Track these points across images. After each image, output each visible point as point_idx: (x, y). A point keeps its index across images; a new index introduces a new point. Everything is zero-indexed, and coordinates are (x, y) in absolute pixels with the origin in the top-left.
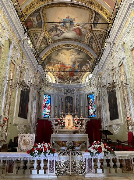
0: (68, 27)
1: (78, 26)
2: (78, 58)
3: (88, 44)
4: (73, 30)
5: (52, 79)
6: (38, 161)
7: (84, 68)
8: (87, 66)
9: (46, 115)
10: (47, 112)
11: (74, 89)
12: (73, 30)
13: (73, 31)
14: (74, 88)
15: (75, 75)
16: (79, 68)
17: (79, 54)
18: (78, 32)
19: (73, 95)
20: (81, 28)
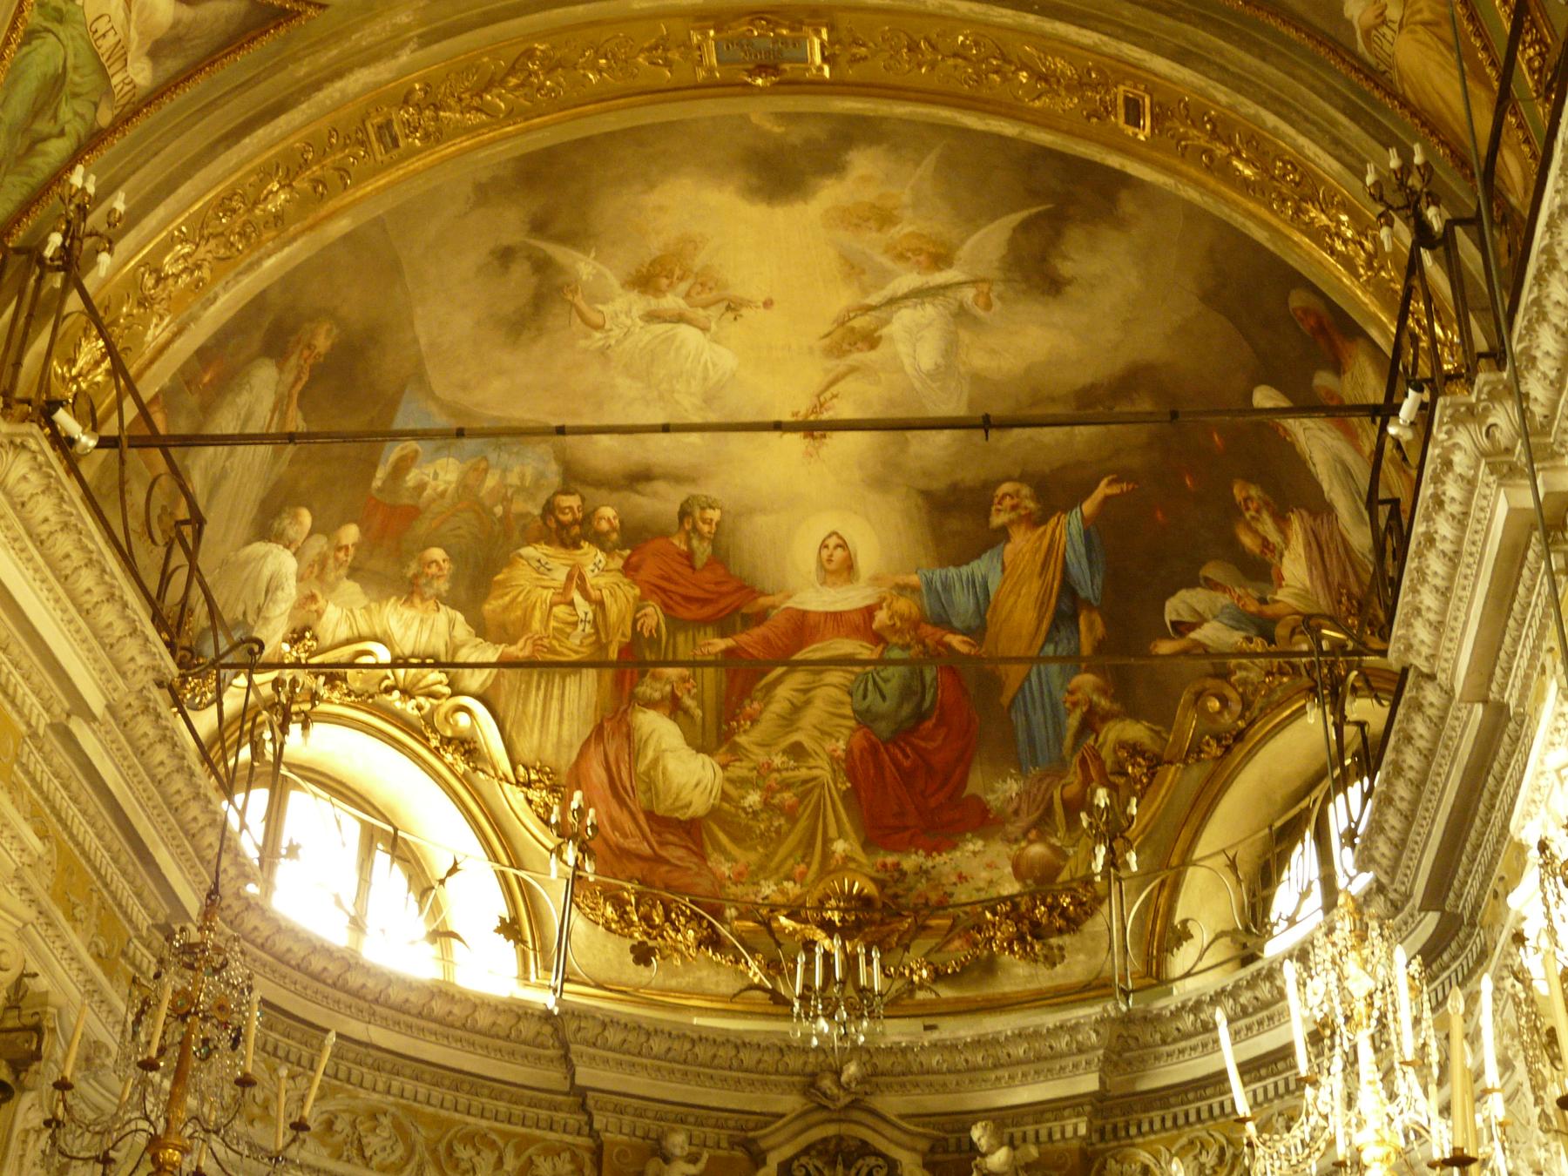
5: (131, 883)
6: (1127, 99)
7: (1211, 633)
8: (1260, 570)
11: (979, 1134)
14: (964, 1120)
15: (983, 821)
16: (1090, 629)
17: (1052, 286)
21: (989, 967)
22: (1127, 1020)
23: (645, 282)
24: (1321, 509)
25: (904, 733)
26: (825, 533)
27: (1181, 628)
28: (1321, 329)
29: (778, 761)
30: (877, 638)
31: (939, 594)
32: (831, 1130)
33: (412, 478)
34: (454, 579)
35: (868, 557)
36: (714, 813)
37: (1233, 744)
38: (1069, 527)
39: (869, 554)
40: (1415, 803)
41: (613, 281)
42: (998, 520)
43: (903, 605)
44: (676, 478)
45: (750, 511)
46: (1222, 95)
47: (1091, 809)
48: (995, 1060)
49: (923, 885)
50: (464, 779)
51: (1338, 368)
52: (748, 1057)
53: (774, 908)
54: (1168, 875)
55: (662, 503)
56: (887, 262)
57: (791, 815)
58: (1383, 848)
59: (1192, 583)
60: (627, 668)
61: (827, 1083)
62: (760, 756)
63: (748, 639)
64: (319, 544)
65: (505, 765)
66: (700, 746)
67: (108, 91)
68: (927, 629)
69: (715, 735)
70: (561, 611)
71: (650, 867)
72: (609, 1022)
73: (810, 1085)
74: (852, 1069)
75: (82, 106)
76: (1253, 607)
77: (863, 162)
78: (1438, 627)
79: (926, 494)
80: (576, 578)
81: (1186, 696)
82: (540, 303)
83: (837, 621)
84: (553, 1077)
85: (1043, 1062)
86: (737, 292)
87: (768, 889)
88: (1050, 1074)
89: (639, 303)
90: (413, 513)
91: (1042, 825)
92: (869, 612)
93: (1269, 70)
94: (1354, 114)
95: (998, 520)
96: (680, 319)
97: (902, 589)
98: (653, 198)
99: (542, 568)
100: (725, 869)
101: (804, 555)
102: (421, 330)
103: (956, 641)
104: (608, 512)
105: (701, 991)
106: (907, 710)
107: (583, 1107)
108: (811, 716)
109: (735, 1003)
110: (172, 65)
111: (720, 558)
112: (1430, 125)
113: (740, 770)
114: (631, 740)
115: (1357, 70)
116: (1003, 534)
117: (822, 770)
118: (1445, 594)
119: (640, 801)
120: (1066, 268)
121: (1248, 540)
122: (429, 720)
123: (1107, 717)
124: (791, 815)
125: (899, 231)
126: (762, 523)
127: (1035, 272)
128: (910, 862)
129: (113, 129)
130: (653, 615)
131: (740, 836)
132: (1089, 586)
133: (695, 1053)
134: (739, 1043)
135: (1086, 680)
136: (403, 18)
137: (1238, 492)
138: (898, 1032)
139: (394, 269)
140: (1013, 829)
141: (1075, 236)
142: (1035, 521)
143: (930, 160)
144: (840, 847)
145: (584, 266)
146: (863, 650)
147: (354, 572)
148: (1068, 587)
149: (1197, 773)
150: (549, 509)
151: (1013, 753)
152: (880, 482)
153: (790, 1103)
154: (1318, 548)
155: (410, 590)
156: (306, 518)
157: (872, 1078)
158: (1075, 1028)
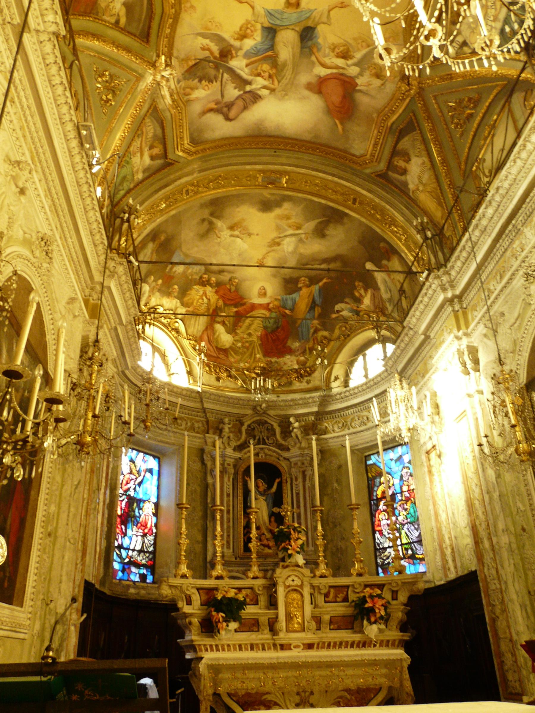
0: (285, 65)
1: (340, 62)
2: (313, 259)
3: (382, 166)
4: (309, 87)
7: (345, 313)
8: (358, 300)
9: (133, 569)
10: (138, 547)
11: (292, 420)
12: (309, 87)
13: (307, 93)
14: (287, 417)
15: (290, 351)
16: (318, 310)
18: (336, 99)
19: (286, 454)
20: (353, 71)
21: (290, 383)
22: (325, 396)
23: (231, 228)
24: (376, 288)
25: (274, 331)
26: (261, 287)
27: (338, 312)
28: (387, 251)
29: (245, 336)
30: (269, 310)
31: (284, 301)
32: (258, 418)
33: (174, 269)
34: (179, 293)
35: (269, 292)
36: (231, 348)
37: (347, 337)
38: (315, 288)
39: (270, 291)
40: (400, 354)
41: (225, 227)
42: (300, 285)
43: (276, 303)
44: (229, 272)
45: (244, 280)
46: (377, 200)
47: (316, 350)
48: (295, 403)
49: (276, 365)
50: (176, 338)
51: (389, 260)
52: (241, 402)
53: (243, 369)
54: (332, 363)
55: (225, 277)
56: (286, 227)
57: (247, 348)
58: (391, 363)
59: (342, 302)
60: (213, 315)
61: (258, 408)
62: (242, 335)
63: (241, 309)
64: (154, 284)
65: (185, 335)
66: (228, 332)
67: (133, 180)
68: (281, 309)
69: (232, 330)
70: (200, 301)
71: (218, 359)
72: (211, 394)
73: (254, 408)
74: (264, 405)
75: (128, 183)
76: (355, 308)
77: (287, 206)
78: (418, 319)
79: (284, 279)
80: (205, 294)
81: (338, 327)
82: (208, 230)
83: (261, 306)
84: (198, 405)
85: (306, 404)
86: (251, 232)
87: (242, 365)
88: (307, 407)
89: (229, 232)
90: (172, 278)
91: (304, 353)
92: (268, 304)
93: (389, 196)
94: (407, 208)
95: (300, 285)
96: (238, 237)
97: (276, 299)
98: (238, 209)
99: (198, 291)
100: (233, 360)
101: (255, 291)
102: (183, 236)
103: (287, 312)
104: (213, 279)
105: (229, 387)
106: (275, 326)
107: (204, 412)
108: (254, 327)
109: (237, 390)
110: (147, 174)
111: (237, 291)
112: (426, 213)
113: (237, 338)
114: (213, 331)
115: (88, 99)
116: (300, 289)
117: (255, 339)
118: (422, 313)
119: (214, 344)
120: (327, 232)
121: (357, 294)
122: (169, 324)
123: (320, 330)
124: (247, 348)
125: (290, 221)
126: (247, 283)
127: (320, 232)
128: (274, 360)
129: (133, 189)
130: (221, 303)
131: (236, 353)
132: (318, 301)
133: (229, 401)
134: (239, 399)
135: (316, 322)
136: (196, 166)
137: (357, 284)
138: (273, 397)
139: (180, 222)
140: (297, 353)
141: (331, 225)
142: (308, 286)
143: (302, 206)
144: (258, 356)
145: (219, 224)
146: (267, 314)
147: (159, 291)
148: (314, 301)
149: (338, 343)
150: (201, 278)
151: (298, 337)
152: (274, 276)
153: (250, 412)
154: (373, 297)
155: (169, 295)
156: (152, 278)
157: (269, 407)
158: (313, 398)
